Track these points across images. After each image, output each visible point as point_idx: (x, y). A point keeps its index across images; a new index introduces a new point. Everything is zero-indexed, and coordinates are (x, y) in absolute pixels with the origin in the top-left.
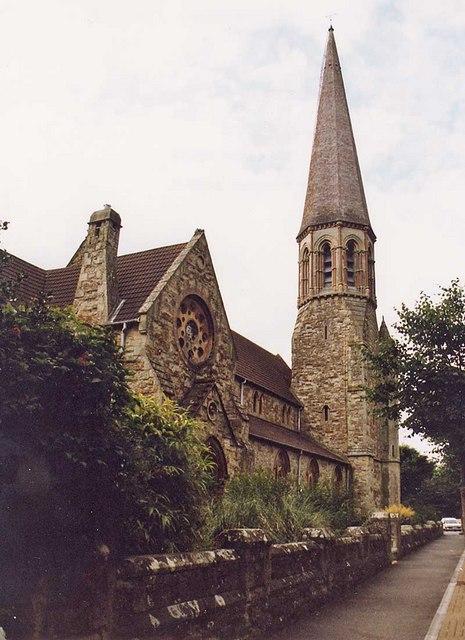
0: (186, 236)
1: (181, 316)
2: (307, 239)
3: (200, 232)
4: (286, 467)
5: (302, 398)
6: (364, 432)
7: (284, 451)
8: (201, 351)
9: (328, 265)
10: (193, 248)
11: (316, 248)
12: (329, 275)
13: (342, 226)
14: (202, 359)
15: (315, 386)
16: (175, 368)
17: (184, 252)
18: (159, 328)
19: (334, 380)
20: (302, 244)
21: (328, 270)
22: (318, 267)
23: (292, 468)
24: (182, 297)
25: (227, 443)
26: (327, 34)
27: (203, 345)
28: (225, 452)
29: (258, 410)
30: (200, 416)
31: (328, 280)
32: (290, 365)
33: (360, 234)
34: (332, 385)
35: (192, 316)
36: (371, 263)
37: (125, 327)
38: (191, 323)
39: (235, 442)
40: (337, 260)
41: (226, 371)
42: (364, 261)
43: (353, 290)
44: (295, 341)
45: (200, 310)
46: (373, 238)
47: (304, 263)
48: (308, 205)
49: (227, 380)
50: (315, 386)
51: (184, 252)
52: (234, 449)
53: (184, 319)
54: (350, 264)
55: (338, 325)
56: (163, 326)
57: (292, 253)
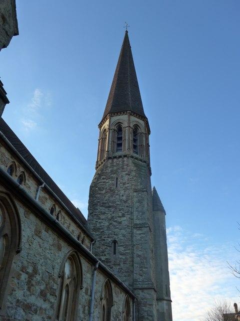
2: (106, 125)
19: (122, 219)
23: (85, 285)
31: (120, 148)
32: (86, 218)
33: (142, 122)
34: (120, 223)
40: (127, 135)
44: (91, 187)
47: (102, 140)
48: (106, 109)
54: (135, 140)
55: (126, 178)
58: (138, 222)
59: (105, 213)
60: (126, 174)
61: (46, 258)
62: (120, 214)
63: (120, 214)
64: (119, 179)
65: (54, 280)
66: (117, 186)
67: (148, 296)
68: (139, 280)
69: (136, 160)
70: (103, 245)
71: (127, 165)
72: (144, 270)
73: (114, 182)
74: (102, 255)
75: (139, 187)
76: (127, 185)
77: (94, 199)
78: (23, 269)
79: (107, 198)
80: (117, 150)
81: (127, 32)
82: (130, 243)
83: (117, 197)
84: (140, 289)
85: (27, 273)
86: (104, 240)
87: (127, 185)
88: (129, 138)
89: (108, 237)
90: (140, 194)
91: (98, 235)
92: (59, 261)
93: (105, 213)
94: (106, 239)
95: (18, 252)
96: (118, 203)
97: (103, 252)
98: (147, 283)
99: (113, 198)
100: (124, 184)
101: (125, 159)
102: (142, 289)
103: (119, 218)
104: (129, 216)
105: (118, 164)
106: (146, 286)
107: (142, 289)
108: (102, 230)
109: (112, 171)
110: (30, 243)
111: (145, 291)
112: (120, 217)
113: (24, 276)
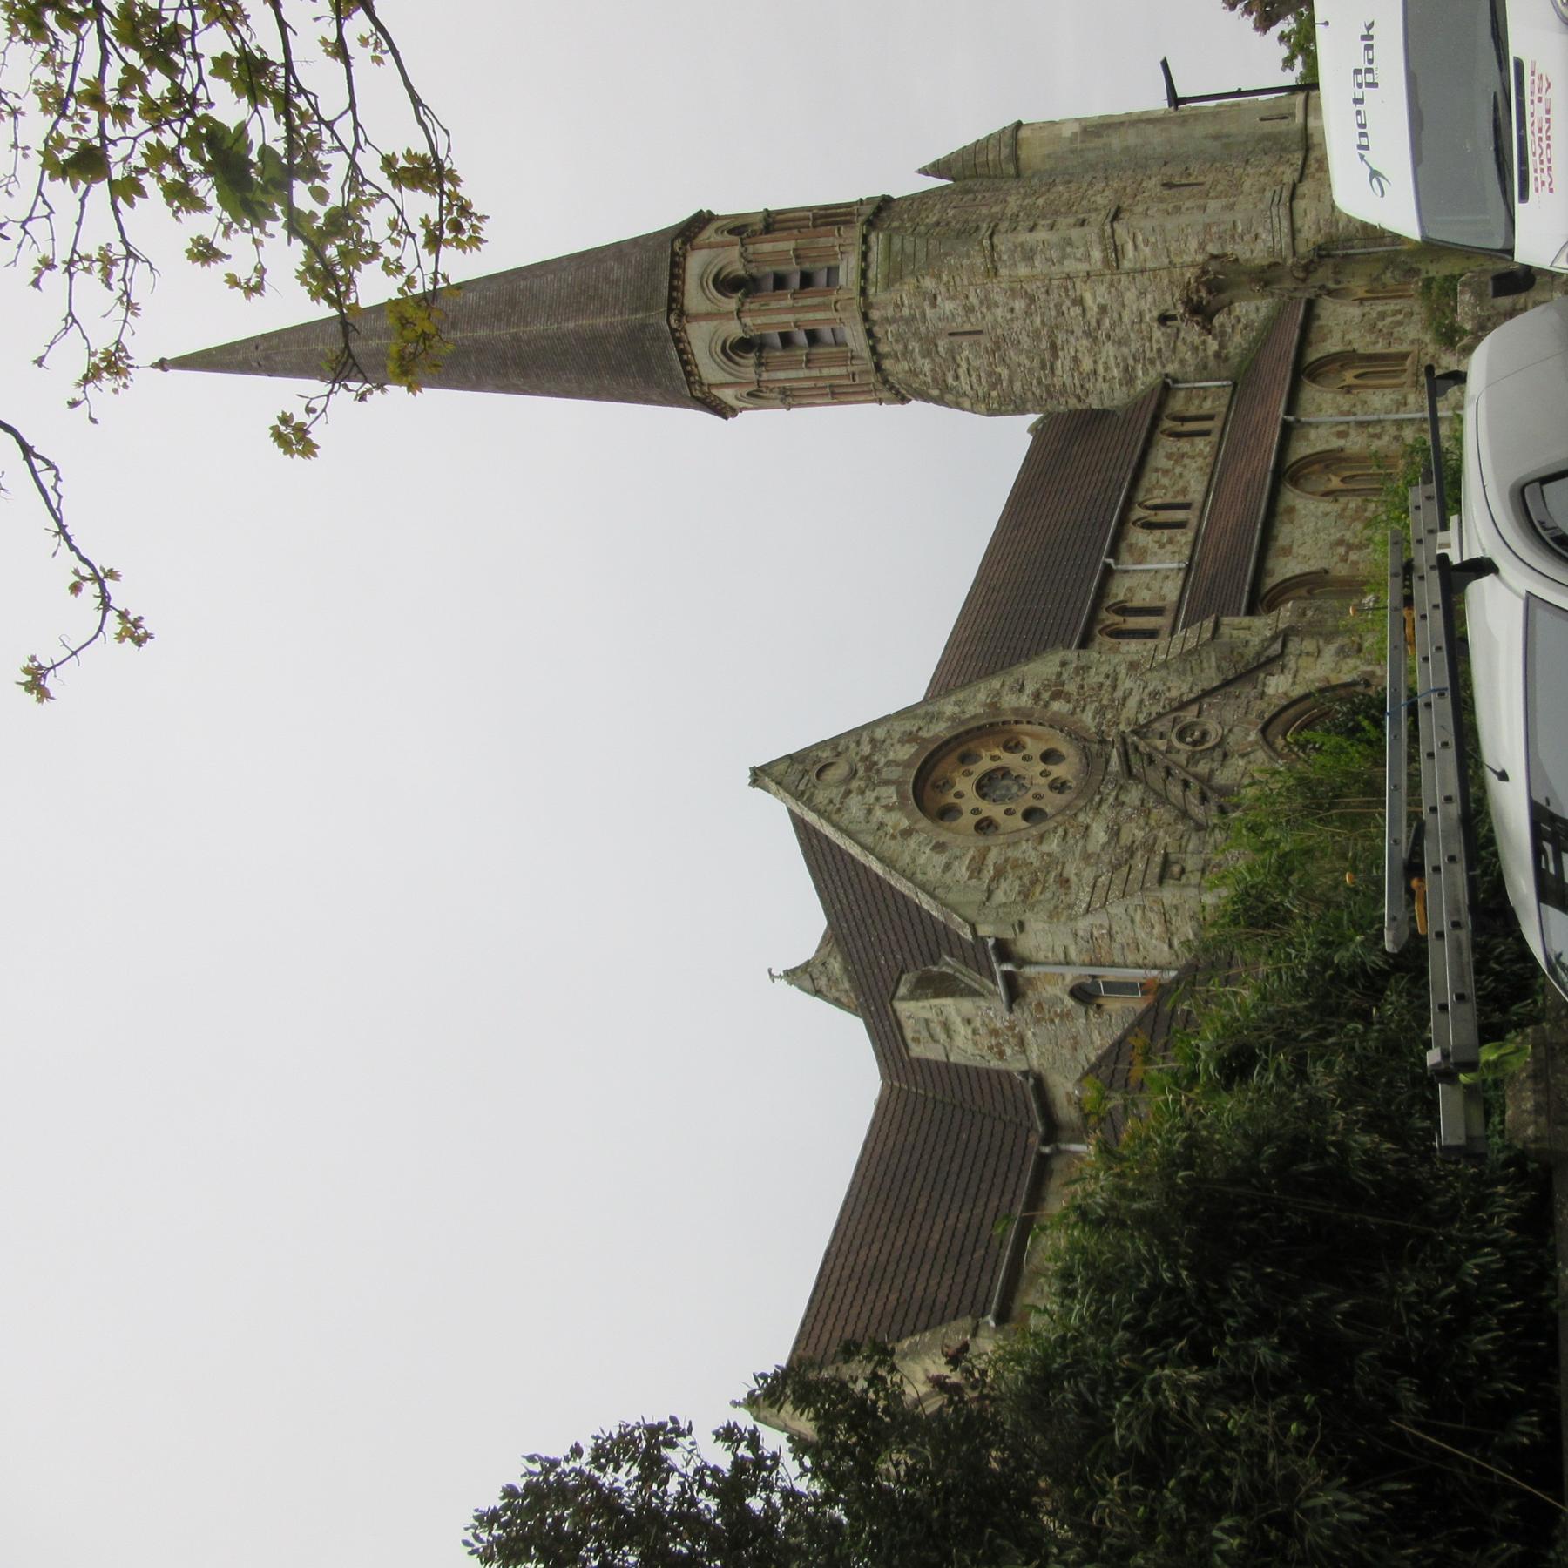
0: (774, 811)
1: (967, 820)
2: (728, 395)
3: (758, 776)
4: (1330, 460)
5: (1145, 379)
6: (1228, 217)
7: (1286, 474)
8: (1049, 757)
9: (787, 339)
10: (798, 796)
11: (750, 373)
12: (813, 337)
13: (682, 314)
14: (1064, 747)
15: (1109, 350)
16: (1099, 835)
17: (811, 817)
18: (1004, 885)
20: (742, 405)
21: (801, 338)
22: (796, 366)
24: (924, 823)
25: (1278, 686)
26: (174, 373)
27: (1034, 748)
28: (1298, 691)
29: (1179, 515)
30: (1212, 772)
31: (827, 335)
33: (695, 263)
34: (1103, 309)
35: (965, 785)
36: (772, 222)
37: (1008, 967)
38: (984, 787)
39: (1271, 660)
41: (1093, 678)
42: (767, 247)
43: (848, 272)
44: (991, 413)
45: (948, 765)
46: (702, 220)
49: (1116, 674)
50: (1109, 350)
51: (811, 817)
52: (1291, 662)
53: (976, 811)
54: (780, 282)
56: (999, 873)
57: (757, 423)
58: (1097, 254)
59: (1075, 359)
60: (934, 305)
61: (1317, 531)
62: (1077, 310)
63: (1077, 310)
64: (955, 327)
65: (1344, 510)
66: (980, 332)
67: (1311, 215)
68: (1270, 244)
69: (871, 274)
70: (1174, 350)
71: (899, 306)
72: (1240, 230)
73: (965, 342)
74: (1205, 350)
75: (979, 261)
76: (974, 300)
77: (1029, 395)
78: (1344, 559)
79: (1023, 359)
80: (837, 344)
81: (162, 365)
82: (1164, 273)
83: (1016, 326)
84: (1294, 239)
85: (1347, 553)
86: (1159, 350)
87: (974, 300)
88: (791, 310)
89: (1150, 339)
90: (1005, 257)
91: (1145, 372)
92: (1312, 507)
93: (1075, 359)
94: (1155, 346)
95: (1326, 572)
96: (1038, 321)
97: (1195, 349)
98: (1276, 220)
99: (1024, 337)
100: (969, 310)
101: (875, 315)
102: (1294, 232)
103: (1088, 315)
104: (1078, 284)
105: (898, 338)
106: (1285, 224)
107: (1294, 232)
108: (1131, 362)
109: (926, 354)
110: (1306, 559)
111: (1298, 224)
112: (1084, 311)
113: (1353, 556)
